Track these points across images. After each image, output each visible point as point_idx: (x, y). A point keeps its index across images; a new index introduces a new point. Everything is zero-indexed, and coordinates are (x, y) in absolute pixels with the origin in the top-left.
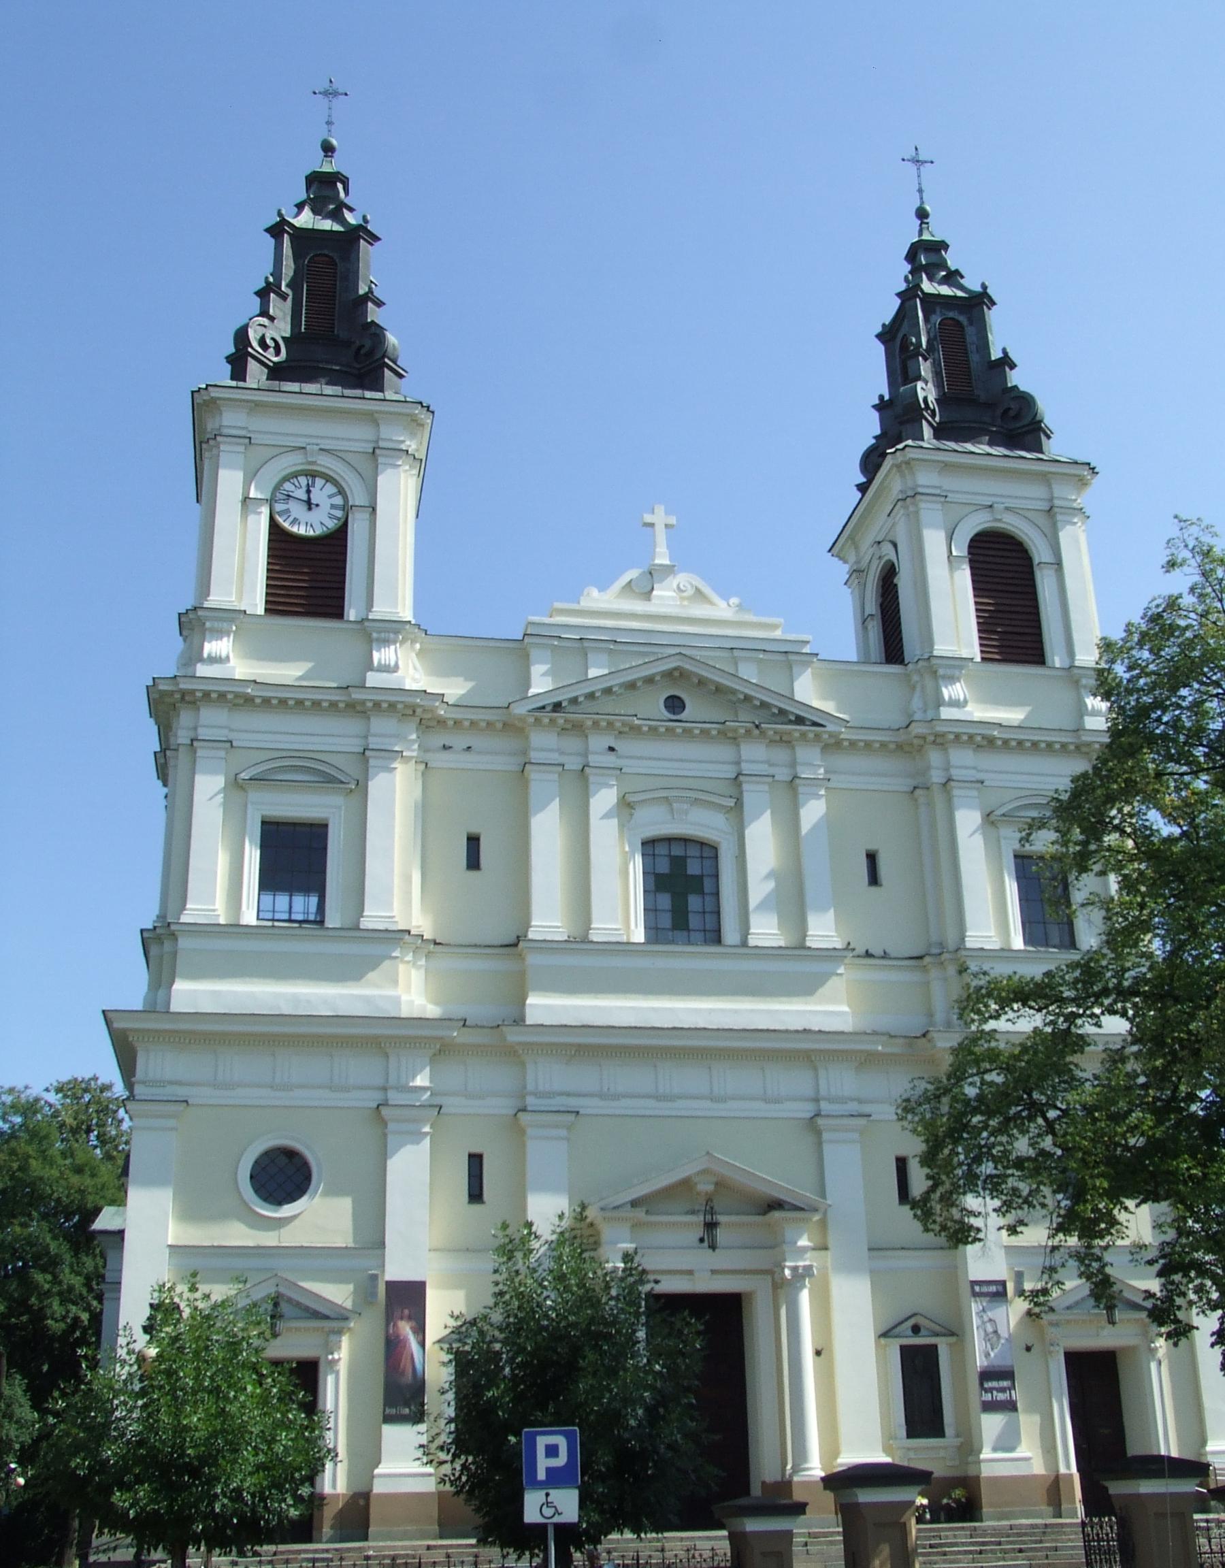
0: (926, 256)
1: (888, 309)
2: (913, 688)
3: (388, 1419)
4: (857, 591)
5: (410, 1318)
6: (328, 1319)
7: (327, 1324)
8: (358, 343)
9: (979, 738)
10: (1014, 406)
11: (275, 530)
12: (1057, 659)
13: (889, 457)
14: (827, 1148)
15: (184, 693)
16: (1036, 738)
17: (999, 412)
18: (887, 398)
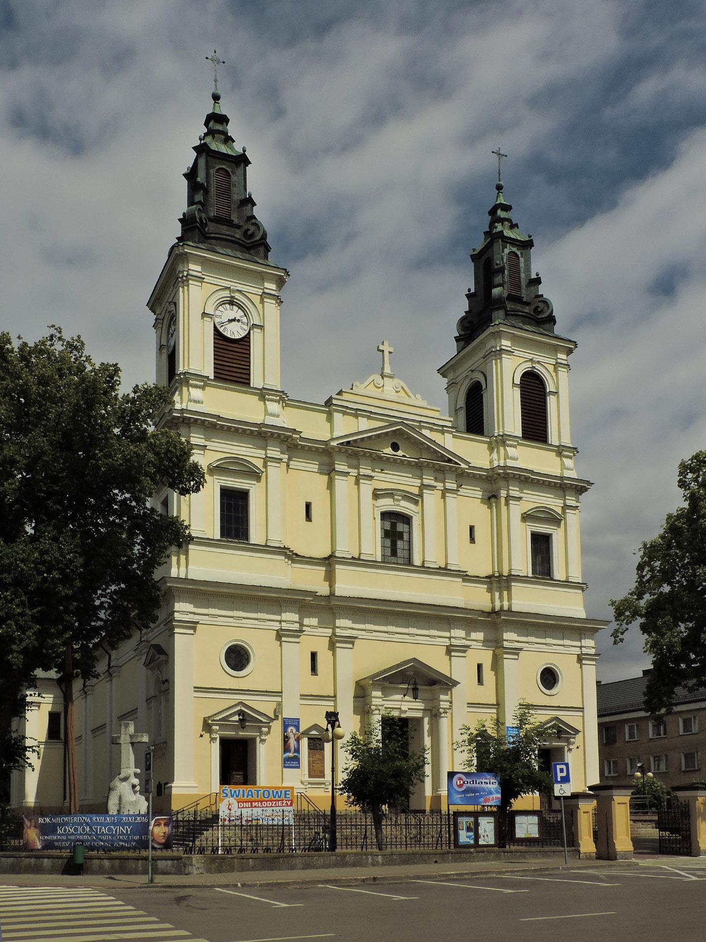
2: (493, 449)
8: (246, 227)
10: (541, 305)
11: (218, 335)
15: (185, 418)
18: (473, 291)
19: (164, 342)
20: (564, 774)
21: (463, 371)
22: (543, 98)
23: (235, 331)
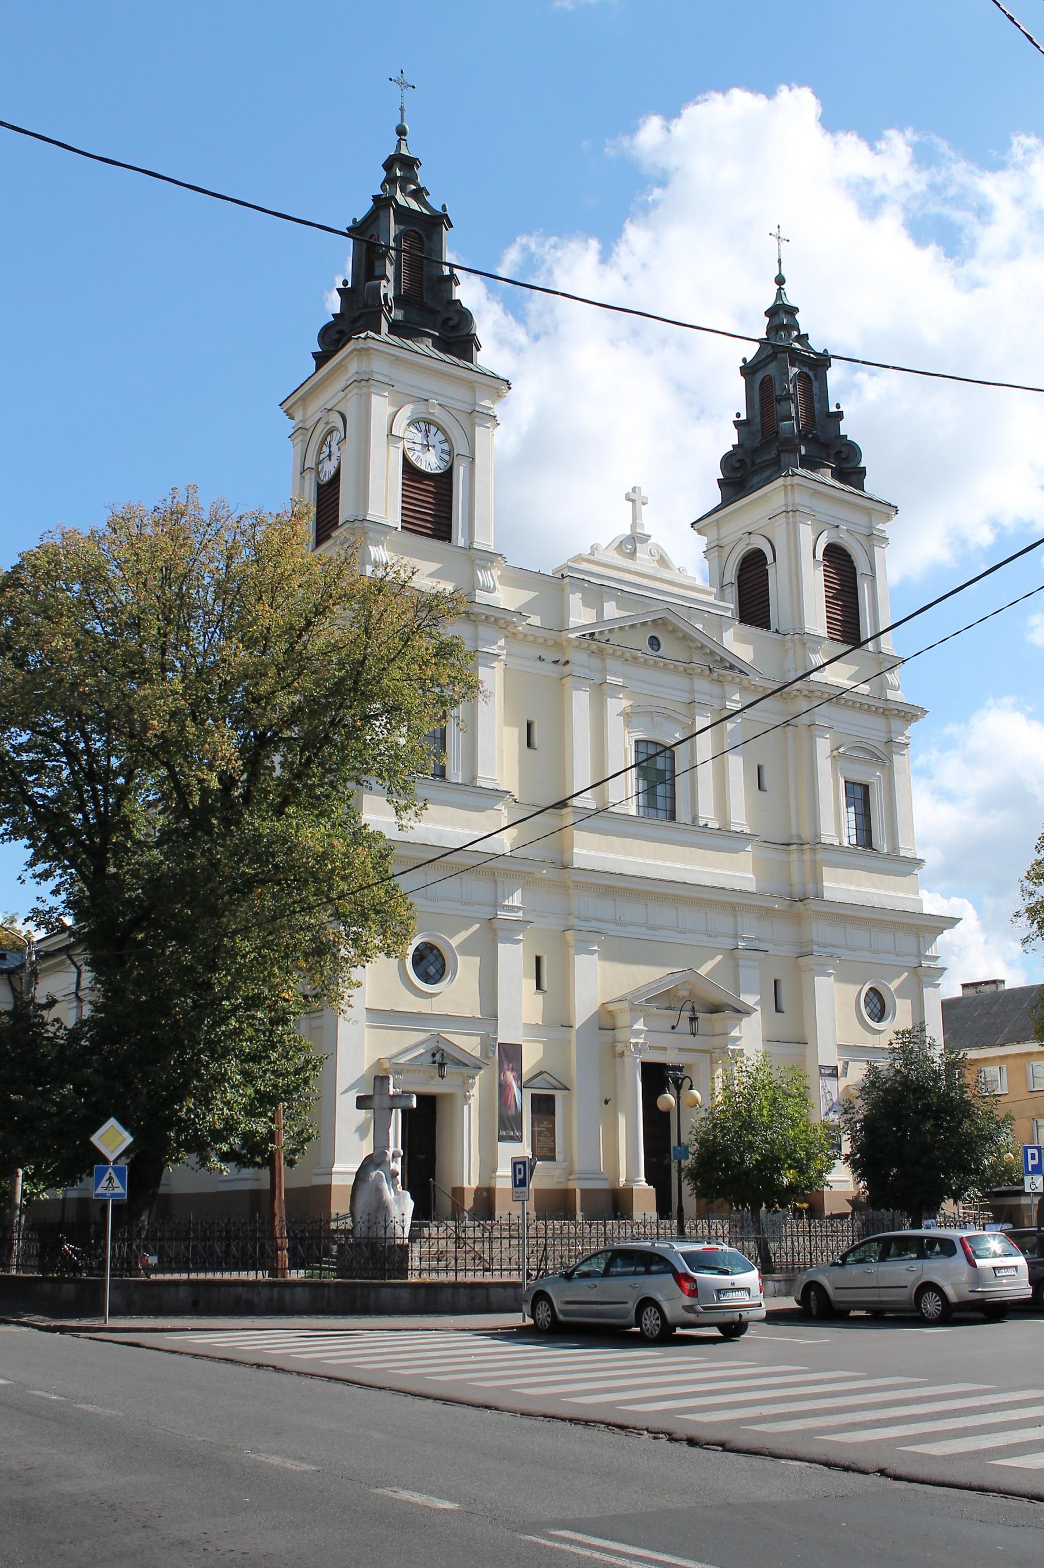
0: (401, 167)
1: (362, 208)
3: (501, 1139)
4: (299, 446)
5: (513, 1070)
6: (467, 1065)
7: (465, 1071)
8: (446, 315)
9: (502, 621)
12: (460, 538)
13: (352, 341)
14: (742, 971)
16: (871, 703)
17: (833, 452)
18: (743, 417)
19: (310, 463)
20: (1036, 1162)
21: (314, 409)
22: (697, 103)
23: (429, 462)
